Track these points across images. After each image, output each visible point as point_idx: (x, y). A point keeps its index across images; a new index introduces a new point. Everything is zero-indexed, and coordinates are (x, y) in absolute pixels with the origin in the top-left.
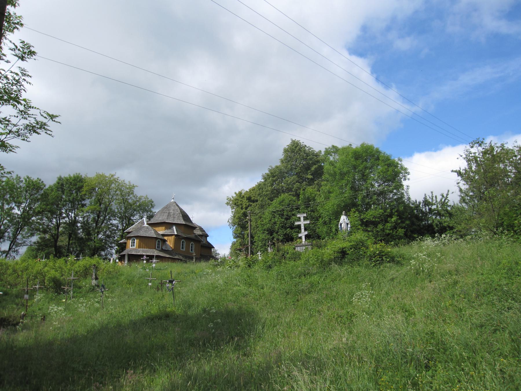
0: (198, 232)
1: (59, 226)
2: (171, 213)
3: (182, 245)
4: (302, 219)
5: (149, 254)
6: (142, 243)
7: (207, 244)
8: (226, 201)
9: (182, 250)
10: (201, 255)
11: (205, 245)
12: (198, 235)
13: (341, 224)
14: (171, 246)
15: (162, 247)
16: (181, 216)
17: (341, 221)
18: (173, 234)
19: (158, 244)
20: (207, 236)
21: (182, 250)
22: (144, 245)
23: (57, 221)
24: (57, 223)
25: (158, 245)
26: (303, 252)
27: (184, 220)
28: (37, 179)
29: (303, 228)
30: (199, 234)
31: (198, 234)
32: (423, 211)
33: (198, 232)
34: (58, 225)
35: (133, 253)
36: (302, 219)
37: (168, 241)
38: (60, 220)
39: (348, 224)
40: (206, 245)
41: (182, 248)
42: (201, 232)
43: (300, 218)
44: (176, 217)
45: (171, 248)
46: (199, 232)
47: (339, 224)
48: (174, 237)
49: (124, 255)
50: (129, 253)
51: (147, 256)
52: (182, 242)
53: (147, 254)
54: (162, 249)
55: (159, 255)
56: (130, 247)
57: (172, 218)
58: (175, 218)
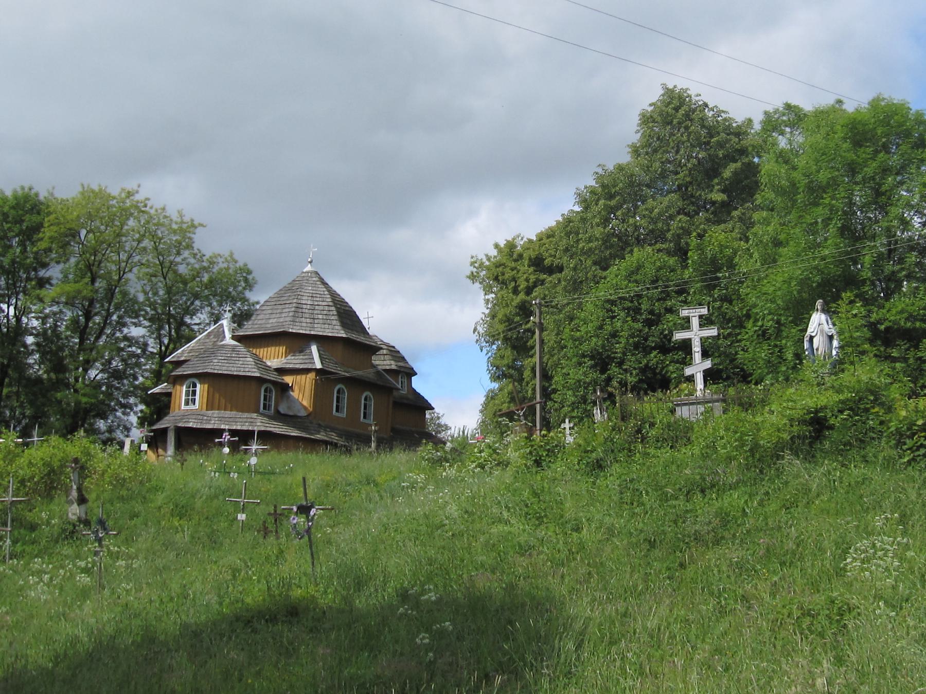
0: (385, 363)
2: (304, 306)
3: (338, 401)
4: (695, 322)
6: (217, 396)
7: (410, 397)
8: (469, 269)
9: (337, 414)
10: (393, 430)
12: (385, 370)
14: (305, 403)
16: (335, 313)
17: (812, 328)
18: (310, 366)
19: (265, 397)
20: (411, 373)
21: (337, 414)
22: (223, 401)
25: (265, 399)
27: (344, 325)
29: (697, 348)
30: (388, 368)
31: (384, 367)
33: (385, 363)
35: (190, 425)
37: (296, 388)
39: (831, 338)
41: (337, 410)
42: (393, 362)
44: (320, 317)
45: (305, 408)
46: (388, 362)
47: (806, 339)
48: (312, 375)
49: (164, 431)
51: (233, 433)
52: (338, 392)
53: (234, 428)
54: (277, 412)
56: (183, 407)
58: (316, 321)
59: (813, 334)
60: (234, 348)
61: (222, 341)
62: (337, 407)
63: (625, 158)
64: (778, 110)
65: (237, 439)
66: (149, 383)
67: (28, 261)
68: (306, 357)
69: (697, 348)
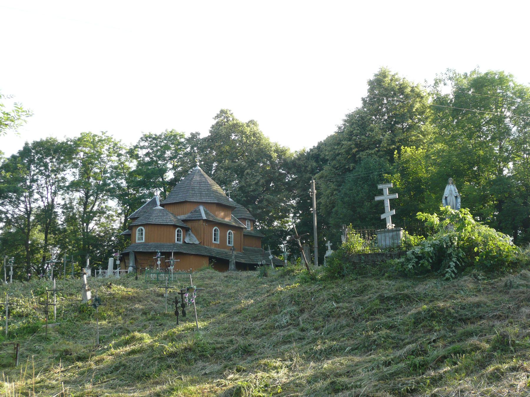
1: (30, 213)
3: (215, 236)
4: (386, 192)
5: (165, 251)
9: (215, 242)
11: (249, 234)
13: (446, 198)
15: (184, 239)
17: (447, 192)
18: (199, 218)
19: (178, 234)
21: (215, 242)
23: (26, 206)
24: (26, 209)
25: (178, 236)
26: (436, 224)
28: (402, 77)
29: (387, 204)
32: (360, 255)
34: (28, 213)
35: (141, 250)
36: (386, 192)
38: (30, 204)
39: (456, 197)
40: (251, 233)
41: (215, 240)
43: (382, 190)
44: (204, 193)
47: (444, 198)
49: (127, 254)
50: (136, 250)
51: (162, 253)
52: (215, 231)
53: (163, 251)
55: (181, 251)
56: (137, 241)
57: (199, 197)
58: (202, 195)
59: (447, 196)
60: (160, 210)
61: (155, 207)
62: (215, 238)
63: (360, 105)
64: (406, 87)
65: (164, 256)
66: (103, 205)
67: (237, 182)
68: (198, 214)
69: (387, 204)
